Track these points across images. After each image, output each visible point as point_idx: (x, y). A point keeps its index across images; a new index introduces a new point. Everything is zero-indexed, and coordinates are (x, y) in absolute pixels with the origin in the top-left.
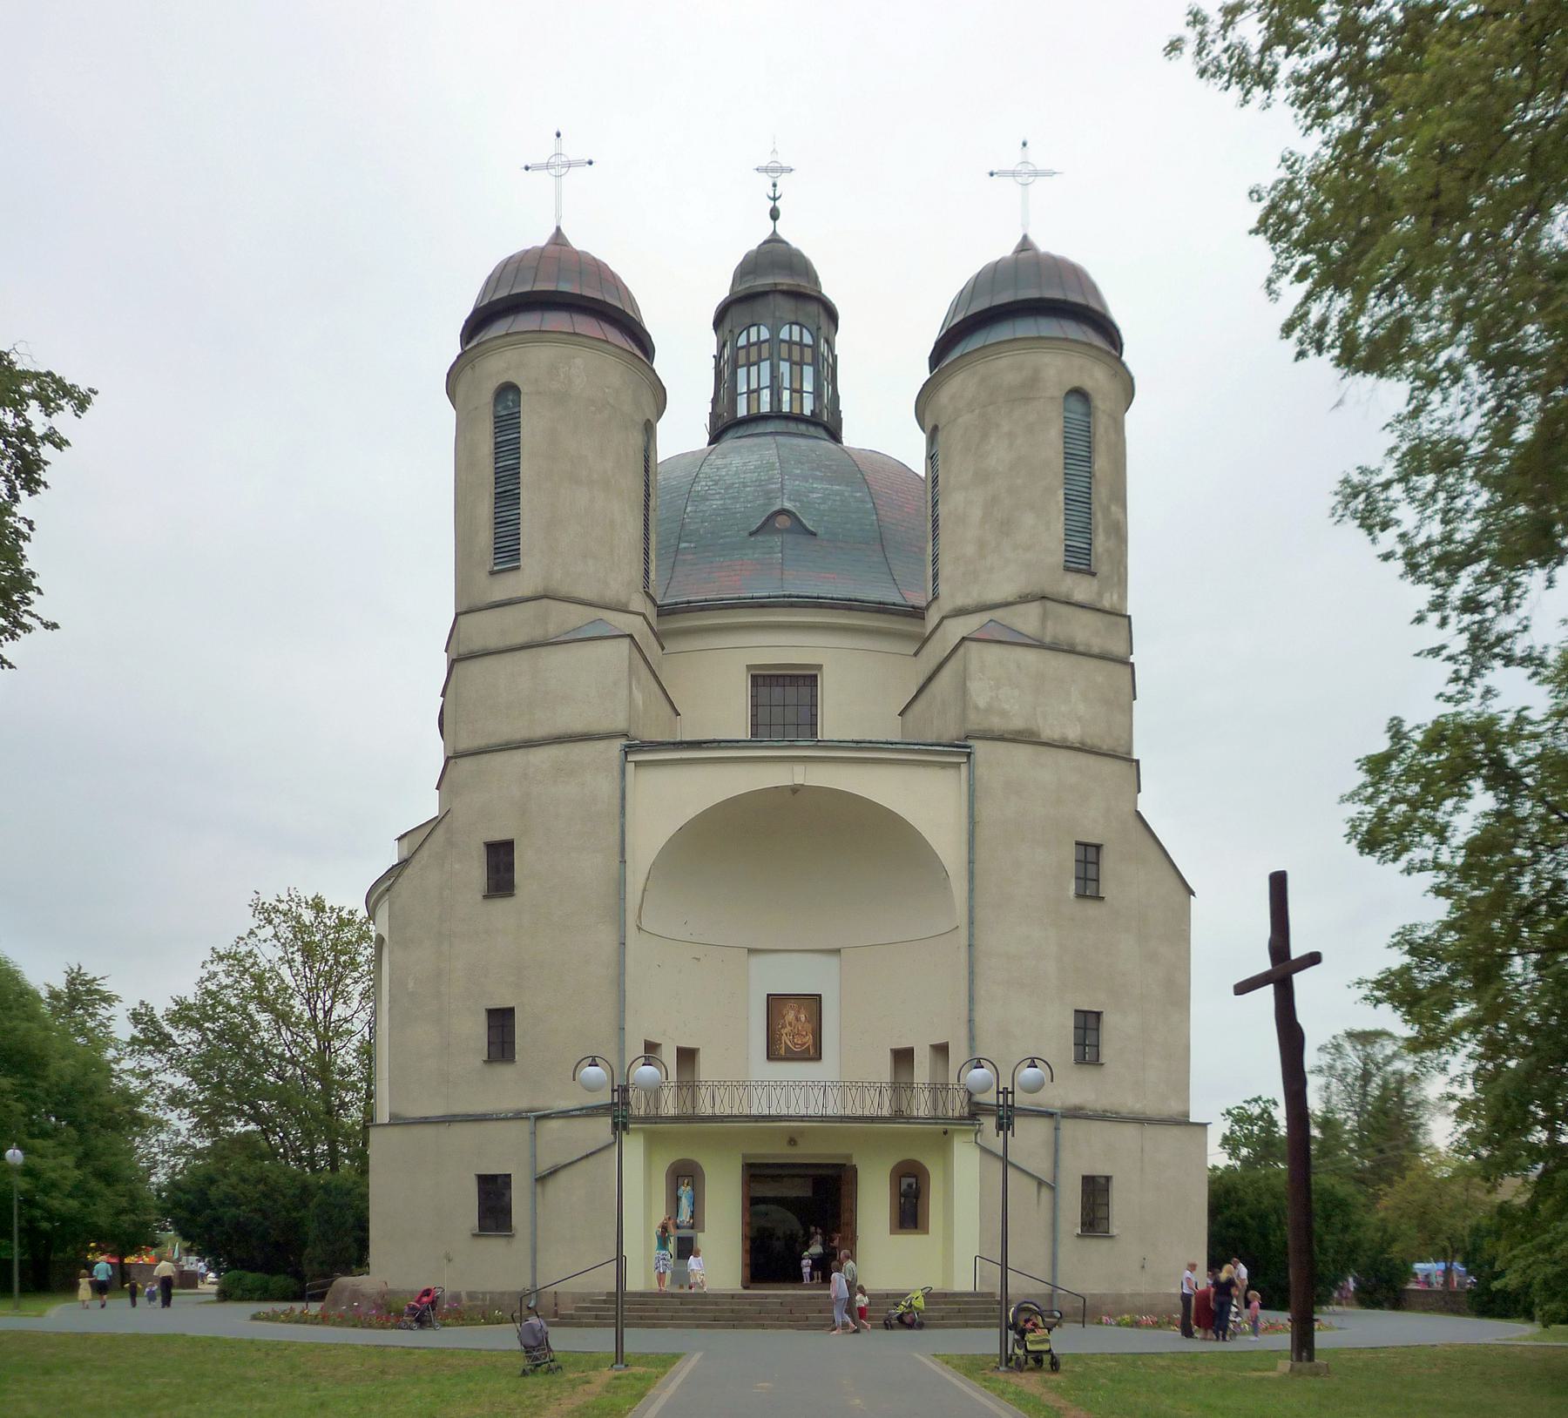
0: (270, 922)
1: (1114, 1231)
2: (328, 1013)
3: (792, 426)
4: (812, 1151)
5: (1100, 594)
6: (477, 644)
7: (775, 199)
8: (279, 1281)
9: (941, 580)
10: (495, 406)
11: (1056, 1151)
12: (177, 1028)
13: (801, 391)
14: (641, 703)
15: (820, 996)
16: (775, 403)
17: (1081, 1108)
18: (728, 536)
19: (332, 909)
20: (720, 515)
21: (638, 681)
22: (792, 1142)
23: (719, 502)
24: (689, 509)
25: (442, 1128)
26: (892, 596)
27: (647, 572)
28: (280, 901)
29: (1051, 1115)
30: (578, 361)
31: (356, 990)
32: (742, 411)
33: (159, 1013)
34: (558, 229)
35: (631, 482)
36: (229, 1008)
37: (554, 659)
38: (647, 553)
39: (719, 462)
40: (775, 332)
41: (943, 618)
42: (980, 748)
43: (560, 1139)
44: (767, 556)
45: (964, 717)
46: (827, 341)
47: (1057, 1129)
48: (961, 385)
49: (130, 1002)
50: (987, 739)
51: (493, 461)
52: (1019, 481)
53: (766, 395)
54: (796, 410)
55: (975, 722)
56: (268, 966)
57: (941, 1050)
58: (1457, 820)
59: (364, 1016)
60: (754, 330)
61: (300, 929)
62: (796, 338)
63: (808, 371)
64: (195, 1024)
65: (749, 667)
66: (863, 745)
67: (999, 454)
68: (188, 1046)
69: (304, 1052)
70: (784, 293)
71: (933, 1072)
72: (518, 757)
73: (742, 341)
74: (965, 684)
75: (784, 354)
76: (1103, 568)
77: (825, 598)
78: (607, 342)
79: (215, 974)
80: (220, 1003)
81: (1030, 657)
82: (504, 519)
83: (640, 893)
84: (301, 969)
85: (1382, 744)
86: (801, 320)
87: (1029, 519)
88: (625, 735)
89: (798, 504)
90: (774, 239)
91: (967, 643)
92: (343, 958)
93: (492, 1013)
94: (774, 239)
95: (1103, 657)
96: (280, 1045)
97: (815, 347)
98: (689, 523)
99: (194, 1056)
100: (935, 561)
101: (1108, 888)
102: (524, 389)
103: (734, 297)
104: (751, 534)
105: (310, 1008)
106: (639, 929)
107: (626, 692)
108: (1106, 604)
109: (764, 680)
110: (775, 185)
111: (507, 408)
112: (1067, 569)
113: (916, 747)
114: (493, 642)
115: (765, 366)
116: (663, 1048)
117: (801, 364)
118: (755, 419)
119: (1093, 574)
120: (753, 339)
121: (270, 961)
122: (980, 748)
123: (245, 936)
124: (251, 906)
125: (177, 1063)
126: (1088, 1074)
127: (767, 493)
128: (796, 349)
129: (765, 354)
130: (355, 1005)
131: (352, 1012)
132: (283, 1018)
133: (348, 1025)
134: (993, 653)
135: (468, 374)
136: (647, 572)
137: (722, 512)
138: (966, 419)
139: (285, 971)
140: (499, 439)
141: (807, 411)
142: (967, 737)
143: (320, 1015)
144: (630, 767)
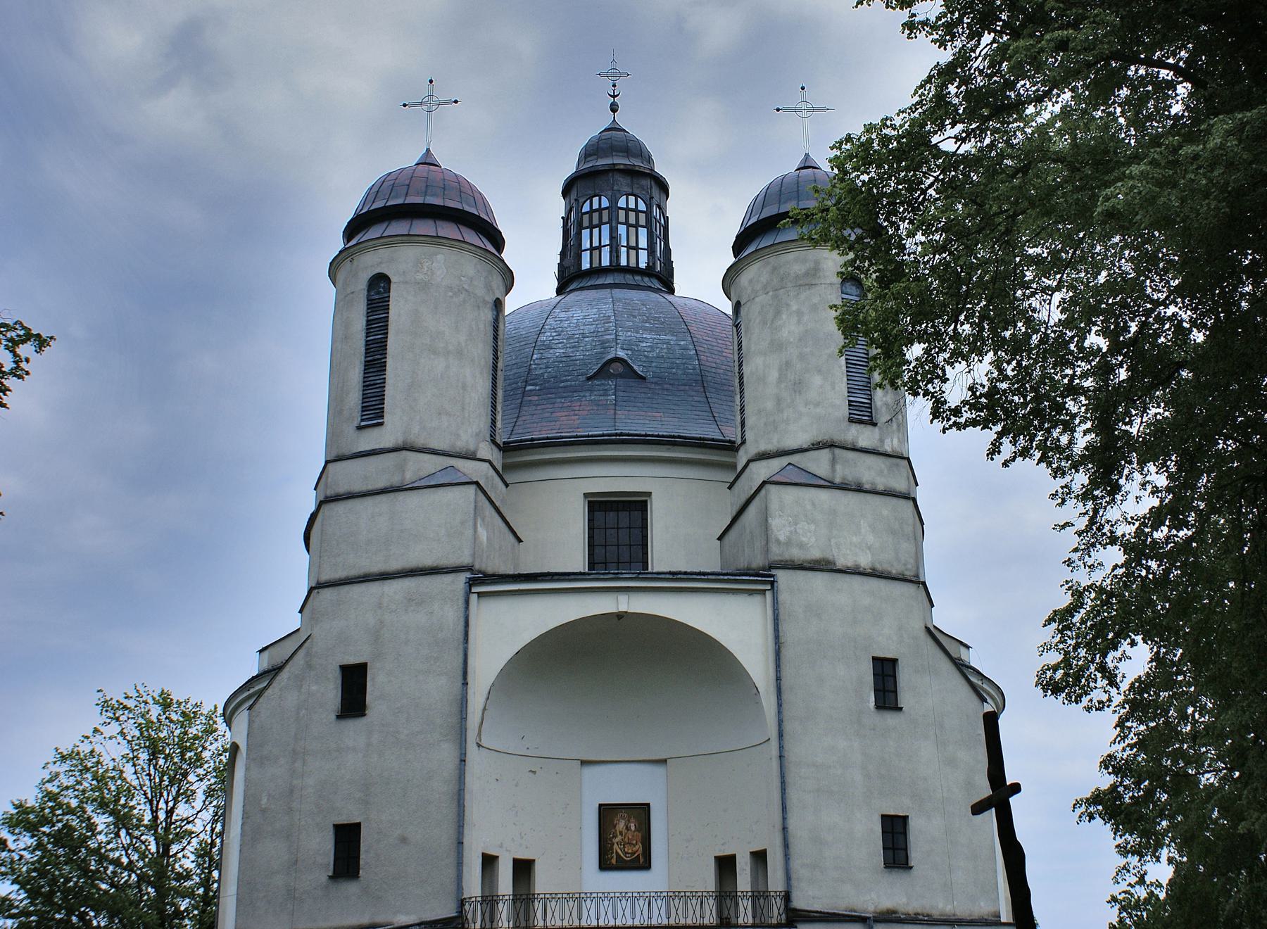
0: (117, 719)
2: (170, 813)
3: (629, 279)
5: (882, 441)
6: (342, 489)
7: (614, 96)
9: (746, 428)
10: (368, 291)
12: (13, 833)
13: (637, 248)
14: (485, 538)
15: (648, 805)
16: (614, 259)
17: (894, 912)
18: (567, 381)
19: (179, 703)
20: (561, 362)
21: (483, 520)
23: (562, 351)
24: (535, 356)
26: (711, 432)
27: (494, 422)
30: (439, 257)
32: (586, 265)
34: (428, 150)
35: (481, 351)
36: (71, 811)
38: (494, 406)
39: (562, 315)
40: (613, 201)
41: (749, 461)
42: (782, 576)
44: (602, 398)
46: (659, 206)
48: (754, 274)
50: (789, 569)
51: (364, 335)
52: (808, 350)
53: (606, 252)
54: (633, 263)
55: (776, 553)
56: (111, 766)
57: (760, 857)
58: (1123, 668)
59: (207, 815)
61: (146, 725)
62: (632, 205)
63: (643, 233)
64: (32, 828)
65: (586, 495)
66: (679, 576)
67: (789, 328)
68: (22, 853)
69: (143, 856)
70: (620, 171)
71: (755, 880)
73: (586, 208)
74: (766, 520)
76: (882, 417)
77: (652, 436)
78: (464, 242)
79: (57, 775)
80: (60, 805)
81: (824, 496)
82: (372, 383)
83: (480, 713)
84: (146, 767)
85: (1066, 600)
86: (636, 191)
87: (817, 380)
88: (469, 568)
89: (630, 352)
90: (614, 128)
91: (768, 486)
92: (189, 754)
94: (614, 128)
95: (887, 493)
96: (117, 849)
97: (648, 213)
98: (535, 368)
99: (27, 863)
100: (742, 411)
101: (905, 699)
102: (393, 279)
103: (577, 174)
104: (589, 379)
105: (151, 809)
106: (479, 745)
108: (888, 448)
109: (598, 506)
110: (614, 86)
111: (379, 293)
112: (851, 421)
113: (726, 578)
114: (358, 487)
115: (605, 228)
116: (501, 861)
117: (637, 226)
118: (597, 271)
119: (875, 425)
120: (595, 206)
121: (113, 759)
124: (97, 705)
127: (603, 343)
128: (632, 215)
129: (605, 218)
130: (198, 804)
132: (123, 820)
133: (189, 827)
134: (790, 494)
135: (346, 266)
136: (494, 422)
137: (564, 359)
138: (762, 299)
139: (129, 771)
140: (370, 318)
141: (643, 265)
142: (770, 568)
144: (474, 598)
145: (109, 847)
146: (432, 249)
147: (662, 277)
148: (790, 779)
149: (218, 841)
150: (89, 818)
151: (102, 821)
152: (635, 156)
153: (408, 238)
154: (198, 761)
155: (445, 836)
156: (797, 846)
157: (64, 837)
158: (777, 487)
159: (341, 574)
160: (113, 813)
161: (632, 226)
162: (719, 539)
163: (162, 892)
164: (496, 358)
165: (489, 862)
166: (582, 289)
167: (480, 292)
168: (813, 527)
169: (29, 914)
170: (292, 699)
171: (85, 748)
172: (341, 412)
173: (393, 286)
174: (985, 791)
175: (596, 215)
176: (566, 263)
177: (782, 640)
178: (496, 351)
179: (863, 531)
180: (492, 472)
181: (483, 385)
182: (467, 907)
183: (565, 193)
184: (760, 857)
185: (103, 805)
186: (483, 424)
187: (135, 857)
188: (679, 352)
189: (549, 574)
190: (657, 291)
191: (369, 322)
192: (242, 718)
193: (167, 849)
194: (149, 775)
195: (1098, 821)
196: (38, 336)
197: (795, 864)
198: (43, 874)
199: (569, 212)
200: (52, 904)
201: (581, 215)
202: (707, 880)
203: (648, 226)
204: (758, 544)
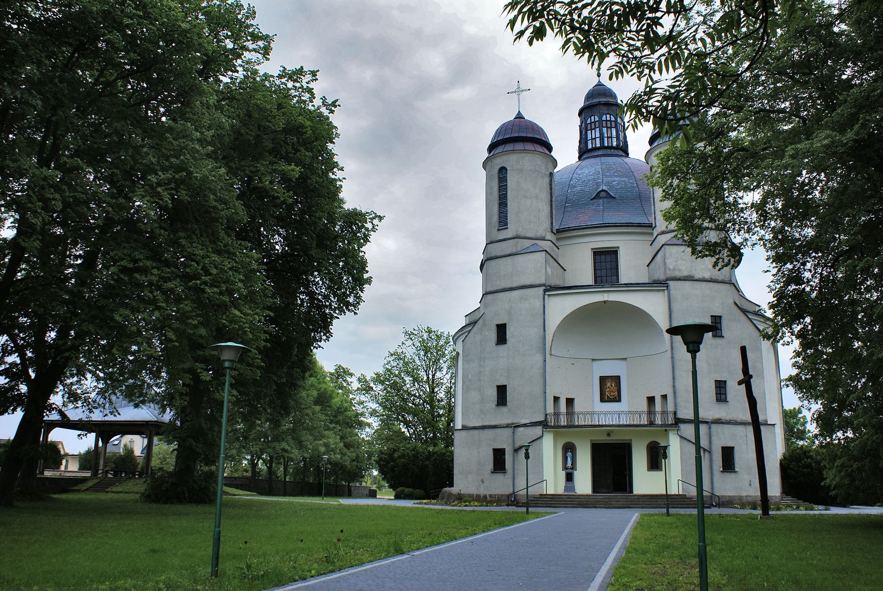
1: (737, 469)
2: (434, 376)
3: (609, 152)
4: (615, 438)
8: (418, 492)
11: (710, 437)
13: (611, 137)
17: (720, 420)
19: (434, 331)
22: (609, 435)
25: (481, 431)
27: (552, 223)
28: (414, 330)
29: (707, 423)
31: (445, 366)
32: (590, 147)
33: (368, 378)
34: (519, 111)
35: (545, 195)
36: (396, 376)
37: (519, 259)
38: (552, 217)
39: (580, 172)
40: (600, 118)
41: (657, 235)
42: (672, 284)
43: (524, 436)
45: (665, 273)
47: (710, 428)
49: (358, 375)
53: (598, 140)
54: (610, 145)
55: (670, 274)
57: (664, 397)
59: (448, 376)
60: (593, 117)
62: (608, 119)
63: (614, 131)
64: (382, 383)
69: (425, 393)
71: (663, 407)
72: (508, 294)
73: (589, 121)
74: (665, 260)
75: (604, 125)
80: (392, 373)
86: (610, 112)
90: (600, 84)
91: (664, 246)
93: (498, 387)
94: (600, 84)
97: (616, 121)
102: (508, 169)
104: (592, 199)
106: (551, 355)
107: (544, 270)
109: (598, 254)
114: (499, 254)
115: (598, 129)
117: (611, 128)
118: (595, 149)
120: (593, 121)
122: (671, 283)
123: (401, 345)
125: (375, 398)
126: (722, 406)
128: (609, 123)
129: (597, 126)
130: (444, 372)
131: (444, 375)
132: (416, 379)
133: (442, 381)
136: (552, 223)
143: (431, 377)
144: (546, 297)
145: (411, 389)
146: (523, 155)
147: (624, 149)
148: (676, 367)
149: (453, 386)
150: (403, 378)
151: (408, 379)
152: (609, 96)
153: (513, 151)
154: (444, 355)
155: (538, 390)
156: (679, 394)
157: (394, 386)
158: (669, 246)
159: (495, 289)
160: (412, 376)
161: (609, 128)
162: (648, 266)
163: (432, 407)
164: (552, 197)
165: (556, 399)
166: (588, 158)
167: (543, 171)
168: (684, 262)
169: (383, 415)
170: (478, 338)
171: (399, 351)
172: (491, 223)
173: (508, 171)
174: (741, 377)
175: (593, 124)
176: (581, 146)
177: (672, 310)
178: (551, 194)
179: (706, 263)
180: (552, 244)
181: (547, 209)
182: (548, 417)
183: (580, 115)
184: (664, 397)
185: (408, 373)
186: (548, 225)
187: (422, 393)
188: (629, 185)
189: (576, 286)
190: (622, 156)
191: (500, 187)
192: (460, 343)
193: (433, 390)
194: (425, 360)
195: (791, 387)
196: (380, 216)
197: (678, 400)
198: (387, 400)
199: (582, 123)
200: (392, 411)
201: (586, 125)
202: (644, 406)
203: (616, 127)
204: (662, 270)
